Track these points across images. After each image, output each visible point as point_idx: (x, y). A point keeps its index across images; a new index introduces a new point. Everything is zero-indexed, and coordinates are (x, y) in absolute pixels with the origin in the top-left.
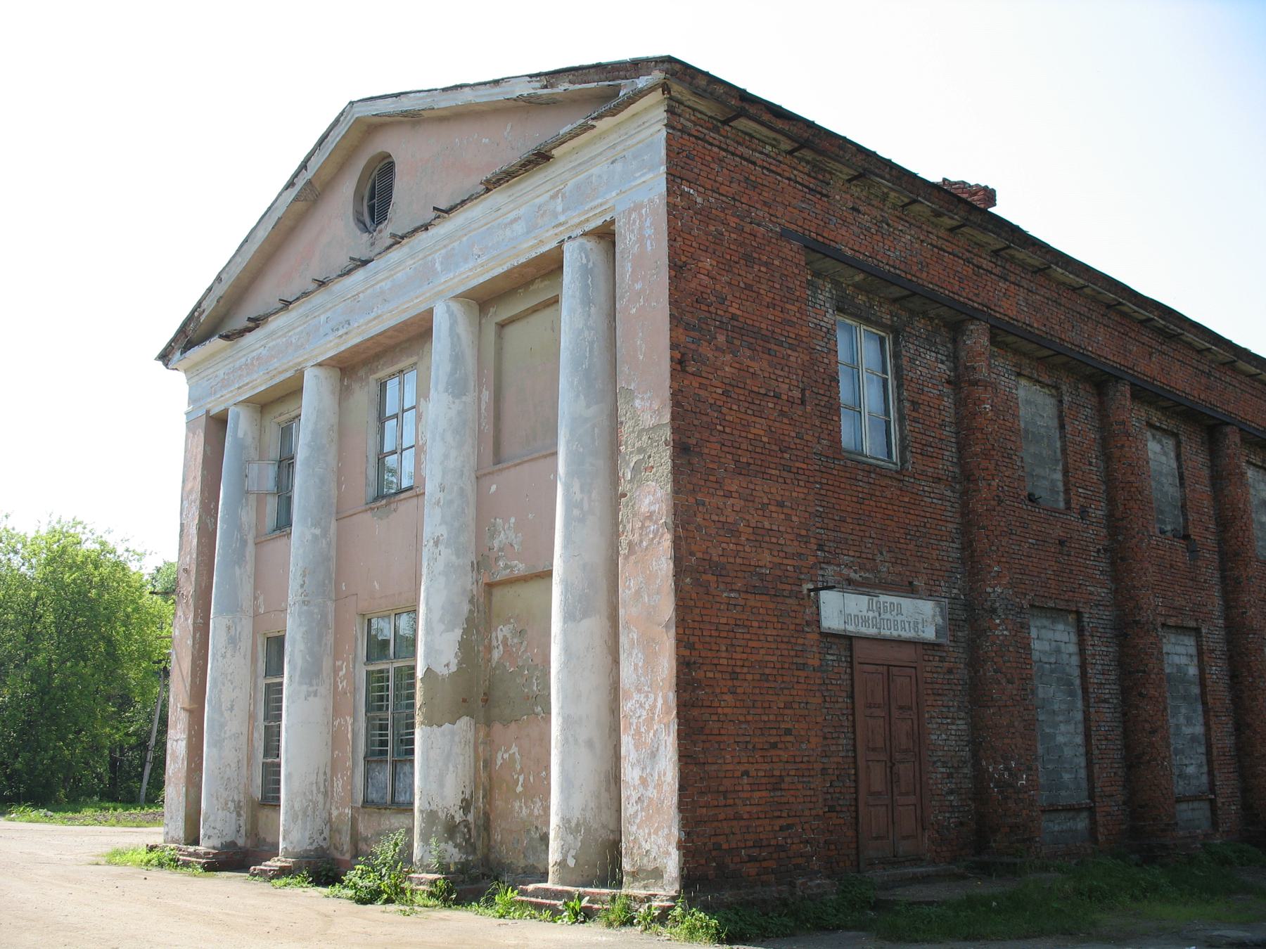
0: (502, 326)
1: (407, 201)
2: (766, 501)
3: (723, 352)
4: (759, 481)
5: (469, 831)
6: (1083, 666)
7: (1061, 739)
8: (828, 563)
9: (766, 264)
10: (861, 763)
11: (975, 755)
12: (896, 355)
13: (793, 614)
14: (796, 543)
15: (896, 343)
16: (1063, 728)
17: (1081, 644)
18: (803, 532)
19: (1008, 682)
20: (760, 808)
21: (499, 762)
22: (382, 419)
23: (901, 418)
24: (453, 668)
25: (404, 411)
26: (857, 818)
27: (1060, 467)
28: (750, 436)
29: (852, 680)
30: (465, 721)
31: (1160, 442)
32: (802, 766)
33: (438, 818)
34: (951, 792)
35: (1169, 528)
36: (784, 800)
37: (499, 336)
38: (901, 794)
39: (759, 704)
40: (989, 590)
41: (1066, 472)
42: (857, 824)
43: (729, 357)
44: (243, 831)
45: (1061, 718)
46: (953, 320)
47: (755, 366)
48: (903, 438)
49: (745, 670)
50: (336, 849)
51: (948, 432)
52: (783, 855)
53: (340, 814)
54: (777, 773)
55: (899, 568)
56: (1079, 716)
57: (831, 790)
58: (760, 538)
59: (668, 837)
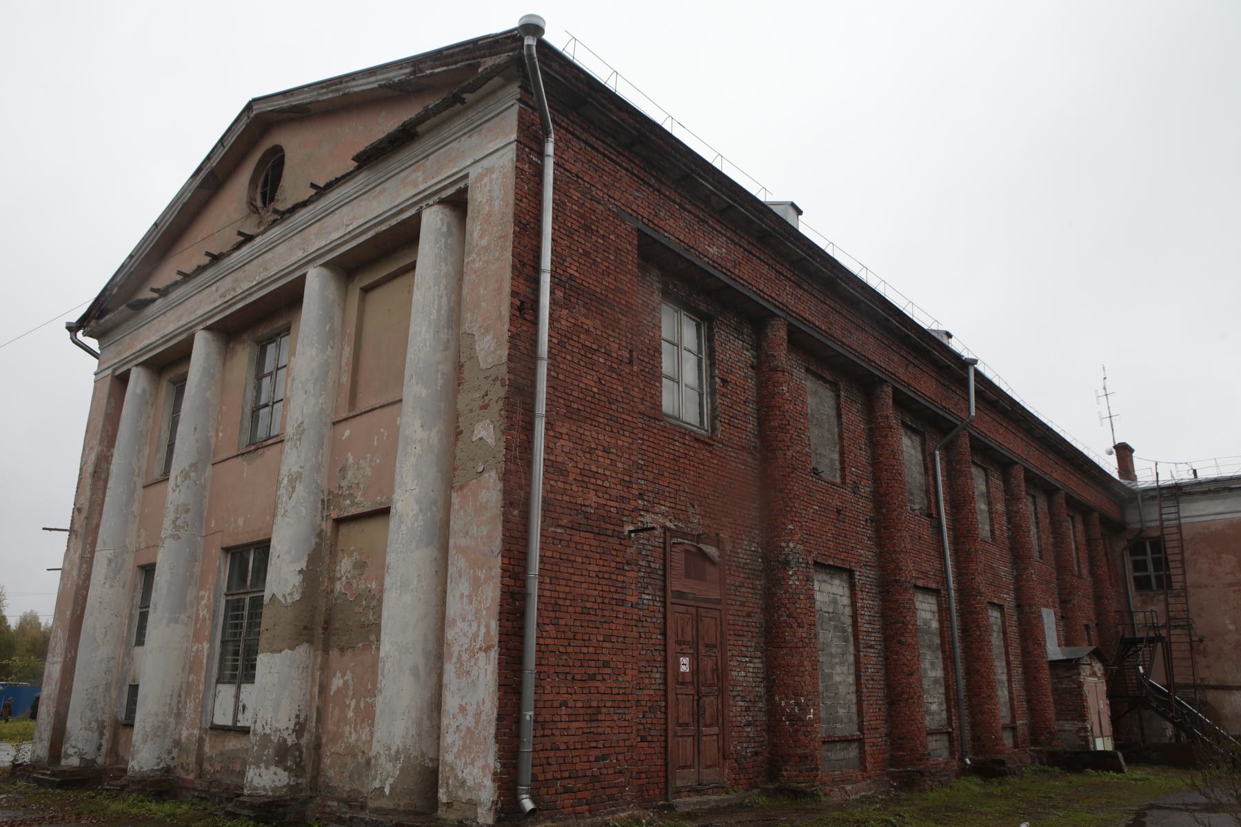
0: (366, 290)
1: (293, 188)
2: (593, 446)
3: (561, 306)
4: (588, 427)
5: (301, 753)
6: (854, 617)
7: (837, 678)
8: (647, 511)
9: (603, 237)
10: (671, 696)
11: (770, 689)
12: (710, 339)
13: (614, 553)
14: (619, 487)
15: (710, 329)
16: (838, 669)
17: (853, 596)
18: (627, 478)
19: (799, 626)
20: (577, 739)
21: (334, 688)
22: (259, 377)
23: (713, 392)
24: (297, 597)
25: (278, 369)
26: (666, 748)
27: (837, 449)
28: (582, 385)
29: (665, 618)
30: (303, 650)
31: (910, 438)
32: (620, 698)
33: (271, 741)
34: (748, 724)
35: (917, 507)
36: (600, 731)
37: (362, 300)
38: (706, 726)
39: (579, 636)
40: (783, 544)
41: (842, 453)
42: (666, 754)
43: (565, 312)
44: (104, 749)
45: (837, 660)
46: (754, 319)
47: (589, 324)
48: (713, 409)
49: (568, 603)
50: (183, 768)
51: (751, 407)
52: (597, 785)
53: (190, 735)
54: (594, 704)
55: (707, 522)
56: (851, 659)
57: (643, 721)
58: (586, 479)
59: (484, 768)
